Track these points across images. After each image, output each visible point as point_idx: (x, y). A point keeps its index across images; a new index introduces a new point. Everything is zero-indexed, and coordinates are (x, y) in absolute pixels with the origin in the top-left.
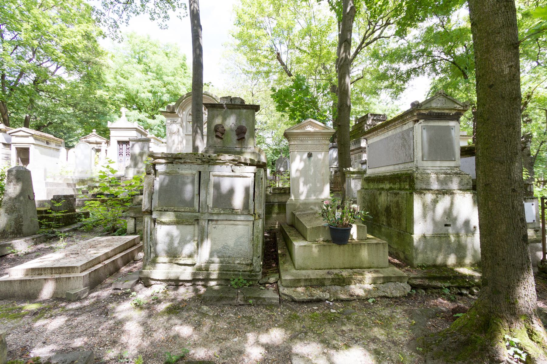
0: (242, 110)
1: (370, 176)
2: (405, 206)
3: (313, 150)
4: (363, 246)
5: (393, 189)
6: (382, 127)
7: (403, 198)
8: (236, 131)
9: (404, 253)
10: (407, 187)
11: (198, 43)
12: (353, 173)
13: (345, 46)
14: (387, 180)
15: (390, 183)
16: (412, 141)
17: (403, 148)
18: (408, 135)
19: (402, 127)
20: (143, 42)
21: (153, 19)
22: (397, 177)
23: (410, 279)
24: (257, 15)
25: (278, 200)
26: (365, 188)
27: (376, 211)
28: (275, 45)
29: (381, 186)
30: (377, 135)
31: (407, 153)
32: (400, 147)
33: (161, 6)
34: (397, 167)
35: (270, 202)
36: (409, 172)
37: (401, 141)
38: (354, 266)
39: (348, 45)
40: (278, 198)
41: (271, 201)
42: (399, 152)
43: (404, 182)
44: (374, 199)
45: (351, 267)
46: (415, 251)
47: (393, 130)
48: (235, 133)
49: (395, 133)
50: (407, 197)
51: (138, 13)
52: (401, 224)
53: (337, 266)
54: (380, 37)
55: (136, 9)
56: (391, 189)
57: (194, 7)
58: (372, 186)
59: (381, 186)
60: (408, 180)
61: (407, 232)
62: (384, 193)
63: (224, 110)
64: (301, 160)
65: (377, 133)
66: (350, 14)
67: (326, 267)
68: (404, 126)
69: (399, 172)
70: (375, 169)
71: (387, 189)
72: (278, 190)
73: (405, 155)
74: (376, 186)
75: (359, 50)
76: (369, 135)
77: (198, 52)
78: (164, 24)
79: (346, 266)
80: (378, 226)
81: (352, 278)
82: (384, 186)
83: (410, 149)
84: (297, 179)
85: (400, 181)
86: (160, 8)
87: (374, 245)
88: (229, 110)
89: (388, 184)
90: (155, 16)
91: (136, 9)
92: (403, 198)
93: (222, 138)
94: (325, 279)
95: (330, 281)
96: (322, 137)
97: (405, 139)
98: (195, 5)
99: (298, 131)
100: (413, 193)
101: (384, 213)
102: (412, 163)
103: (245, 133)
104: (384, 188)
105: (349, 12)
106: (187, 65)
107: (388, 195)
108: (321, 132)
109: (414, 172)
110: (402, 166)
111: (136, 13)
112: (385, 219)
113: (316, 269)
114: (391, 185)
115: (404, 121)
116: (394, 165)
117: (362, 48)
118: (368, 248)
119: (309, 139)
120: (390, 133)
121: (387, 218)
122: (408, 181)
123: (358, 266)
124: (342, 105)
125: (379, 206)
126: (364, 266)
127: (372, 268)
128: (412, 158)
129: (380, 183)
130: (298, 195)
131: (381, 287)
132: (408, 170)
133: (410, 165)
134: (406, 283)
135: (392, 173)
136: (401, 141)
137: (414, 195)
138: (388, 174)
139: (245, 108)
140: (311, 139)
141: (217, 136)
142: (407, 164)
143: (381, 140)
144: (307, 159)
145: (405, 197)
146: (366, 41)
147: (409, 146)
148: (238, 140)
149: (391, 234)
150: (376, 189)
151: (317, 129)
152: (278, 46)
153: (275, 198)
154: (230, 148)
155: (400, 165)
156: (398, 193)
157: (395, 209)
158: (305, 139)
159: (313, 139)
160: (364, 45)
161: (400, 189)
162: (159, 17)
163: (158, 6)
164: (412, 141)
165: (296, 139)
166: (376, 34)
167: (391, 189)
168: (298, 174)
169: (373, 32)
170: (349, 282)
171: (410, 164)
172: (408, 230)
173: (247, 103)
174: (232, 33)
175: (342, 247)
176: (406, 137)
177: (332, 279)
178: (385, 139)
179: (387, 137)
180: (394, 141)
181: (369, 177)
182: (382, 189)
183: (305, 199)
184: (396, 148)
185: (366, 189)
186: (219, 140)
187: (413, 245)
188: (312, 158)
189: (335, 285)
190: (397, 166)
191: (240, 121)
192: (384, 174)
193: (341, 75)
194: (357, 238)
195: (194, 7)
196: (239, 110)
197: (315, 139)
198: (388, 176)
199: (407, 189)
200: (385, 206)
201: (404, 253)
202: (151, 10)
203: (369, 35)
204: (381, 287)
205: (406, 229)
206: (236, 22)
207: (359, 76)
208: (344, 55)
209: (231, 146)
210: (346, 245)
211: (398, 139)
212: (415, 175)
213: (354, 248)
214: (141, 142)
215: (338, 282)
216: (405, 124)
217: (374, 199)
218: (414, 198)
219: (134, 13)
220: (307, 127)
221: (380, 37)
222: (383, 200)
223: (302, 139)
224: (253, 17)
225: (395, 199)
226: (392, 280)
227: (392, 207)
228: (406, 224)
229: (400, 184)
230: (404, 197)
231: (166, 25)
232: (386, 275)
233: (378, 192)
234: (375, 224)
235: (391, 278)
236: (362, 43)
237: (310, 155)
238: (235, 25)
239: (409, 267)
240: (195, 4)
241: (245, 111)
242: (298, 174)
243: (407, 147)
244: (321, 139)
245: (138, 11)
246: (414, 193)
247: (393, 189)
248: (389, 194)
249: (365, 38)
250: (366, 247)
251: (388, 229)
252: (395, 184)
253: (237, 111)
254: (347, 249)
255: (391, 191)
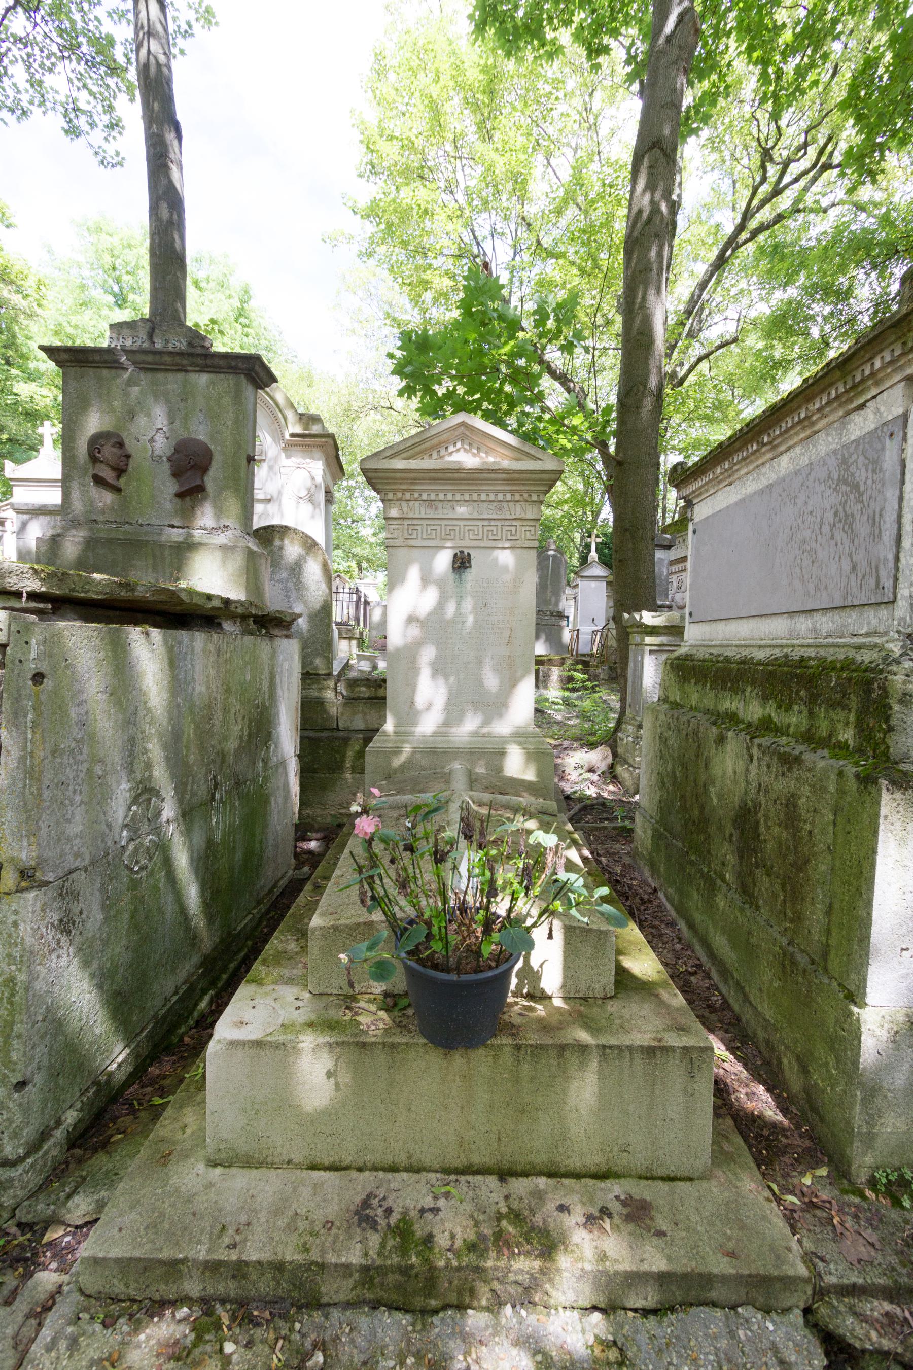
0: (193, 377)
1: (693, 651)
2: (830, 839)
3: (475, 543)
4: (573, 1059)
5: (779, 731)
6: (751, 441)
7: (819, 789)
8: (169, 460)
9: (805, 1070)
10: (847, 735)
11: (164, 182)
12: (653, 631)
13: (651, 167)
14: (753, 683)
15: (765, 698)
16: (891, 494)
17: (839, 535)
18: (875, 465)
19: (844, 425)
20: (130, 246)
21: (73, 131)
22: (800, 677)
23: (821, 1293)
24: (419, 142)
25: (366, 721)
26: (671, 699)
27: (702, 808)
28: (478, 243)
29: (730, 704)
30: (728, 479)
31: (859, 557)
32: (826, 529)
33: (95, 89)
34: (803, 625)
35: (338, 729)
36: (866, 657)
37: (832, 499)
38: (522, 1160)
39: (662, 160)
40: (365, 714)
41: (341, 726)
42: (820, 554)
43: (833, 705)
44: (697, 756)
45: (506, 1166)
46: (866, 1101)
47: (798, 450)
48: (166, 468)
49: (805, 461)
50: (842, 792)
51: (24, 112)
52: (798, 918)
53: (427, 1157)
54: (796, 210)
55: (19, 96)
56: (768, 728)
57: (149, 52)
58: (694, 699)
59: (730, 704)
60: (854, 702)
61: (826, 970)
62: (734, 743)
63: (126, 375)
64: (426, 580)
65: (730, 472)
66: (675, 41)
67: (370, 1158)
68: (857, 418)
69: (812, 653)
70: (714, 625)
71: (750, 725)
72: (368, 687)
73: (846, 566)
74: (709, 702)
75: (729, 253)
76: (699, 483)
77: (165, 213)
78: (110, 148)
79: (477, 1159)
80: (701, 871)
81: (478, 1270)
82: (741, 706)
83: (875, 535)
84: (410, 653)
85: (813, 700)
86: (91, 93)
87: (637, 1056)
88: (142, 375)
89: (755, 703)
90: (82, 122)
91: (19, 96)
92: (819, 789)
93: (118, 490)
94: (322, 1266)
95: (350, 1282)
96: (512, 492)
97: (856, 487)
98: (155, 46)
99: (413, 464)
100: (875, 782)
101: (729, 829)
102: (884, 612)
103: (205, 469)
104: (741, 715)
105: (673, 33)
106: (252, 315)
107: (751, 757)
108: (505, 471)
109: (888, 659)
110: (826, 624)
111: (19, 112)
112: (732, 859)
113: (313, 1167)
114: (770, 709)
115: (857, 388)
116: (791, 614)
117: (738, 246)
118: (600, 1072)
119: (458, 497)
120: (785, 464)
121: (741, 858)
122: (854, 706)
123: (540, 1159)
124: (631, 390)
125: (712, 790)
126: (575, 1163)
127: (617, 1176)
128: (888, 583)
129: (724, 688)
130: (410, 715)
131: (643, 1338)
132: (858, 648)
133: (873, 619)
134: (797, 1317)
135: (778, 653)
136: (832, 499)
137: (885, 797)
138: (760, 655)
139: (203, 369)
140: (467, 497)
141: (99, 481)
142: (854, 615)
143: (742, 501)
144: (451, 576)
145: (832, 788)
146: (753, 224)
147: (875, 521)
148: (180, 495)
149: (753, 940)
150: (707, 712)
151: (491, 459)
152: (487, 246)
153: (355, 713)
154: (149, 529)
155: (817, 617)
156: (798, 760)
157: (776, 830)
158: (441, 496)
159: (475, 496)
160: (744, 236)
161: (809, 738)
162: (93, 125)
163: (85, 86)
164: (891, 494)
165: (408, 496)
166: (784, 202)
167: (766, 726)
168: (415, 632)
169: (777, 192)
170: (460, 1293)
171: (870, 613)
172: (834, 963)
173: (219, 346)
174: (350, 204)
175: (458, 1060)
176: (861, 475)
177: (365, 1269)
178: (761, 492)
179: (770, 487)
180: (800, 501)
181: (688, 657)
182: (733, 717)
183: (435, 734)
184: (807, 534)
185: (675, 705)
186: (108, 497)
187: (856, 1062)
188: (470, 575)
189: (375, 1305)
190: (802, 619)
191: (186, 418)
192: (745, 652)
193: (633, 276)
194: (564, 986)
195: (149, 52)
196: (180, 376)
197: (483, 497)
198: (760, 663)
199: (844, 746)
200: (737, 800)
201: (805, 1070)
202: (64, 100)
203: (763, 203)
204: (643, 1338)
205: (825, 955)
206: (363, 166)
207: (728, 337)
208: (647, 197)
209: (154, 521)
210: (481, 1051)
211: (819, 488)
212: (900, 678)
213: (526, 1068)
214: (47, 518)
215: (399, 1287)
216: (862, 406)
217: (697, 756)
218: (884, 811)
219: (12, 111)
220: (451, 449)
221: (796, 210)
222: (730, 771)
223: (433, 497)
224: (409, 146)
225: (782, 786)
226: (714, 1295)
227: (766, 817)
228: (828, 932)
229: (811, 714)
230: (824, 789)
231: (118, 154)
232: (684, 1265)
233: (714, 729)
234: (692, 863)
235: (707, 1280)
236: (741, 228)
237: (461, 563)
238: (361, 176)
239: (823, 1172)
240: (152, 41)
241: (203, 379)
242: (415, 632)
243: (863, 529)
244: (509, 497)
245: (25, 104)
246: (884, 783)
247: (779, 731)
248: (755, 751)
249: (747, 215)
250: (594, 1064)
251: (742, 910)
252: (789, 709)
253: (173, 382)
254: (485, 1070)
255: (766, 741)
